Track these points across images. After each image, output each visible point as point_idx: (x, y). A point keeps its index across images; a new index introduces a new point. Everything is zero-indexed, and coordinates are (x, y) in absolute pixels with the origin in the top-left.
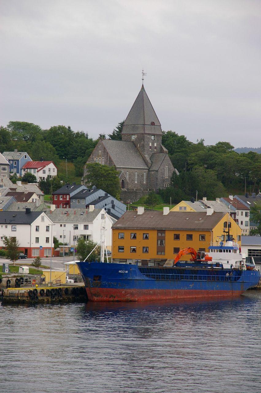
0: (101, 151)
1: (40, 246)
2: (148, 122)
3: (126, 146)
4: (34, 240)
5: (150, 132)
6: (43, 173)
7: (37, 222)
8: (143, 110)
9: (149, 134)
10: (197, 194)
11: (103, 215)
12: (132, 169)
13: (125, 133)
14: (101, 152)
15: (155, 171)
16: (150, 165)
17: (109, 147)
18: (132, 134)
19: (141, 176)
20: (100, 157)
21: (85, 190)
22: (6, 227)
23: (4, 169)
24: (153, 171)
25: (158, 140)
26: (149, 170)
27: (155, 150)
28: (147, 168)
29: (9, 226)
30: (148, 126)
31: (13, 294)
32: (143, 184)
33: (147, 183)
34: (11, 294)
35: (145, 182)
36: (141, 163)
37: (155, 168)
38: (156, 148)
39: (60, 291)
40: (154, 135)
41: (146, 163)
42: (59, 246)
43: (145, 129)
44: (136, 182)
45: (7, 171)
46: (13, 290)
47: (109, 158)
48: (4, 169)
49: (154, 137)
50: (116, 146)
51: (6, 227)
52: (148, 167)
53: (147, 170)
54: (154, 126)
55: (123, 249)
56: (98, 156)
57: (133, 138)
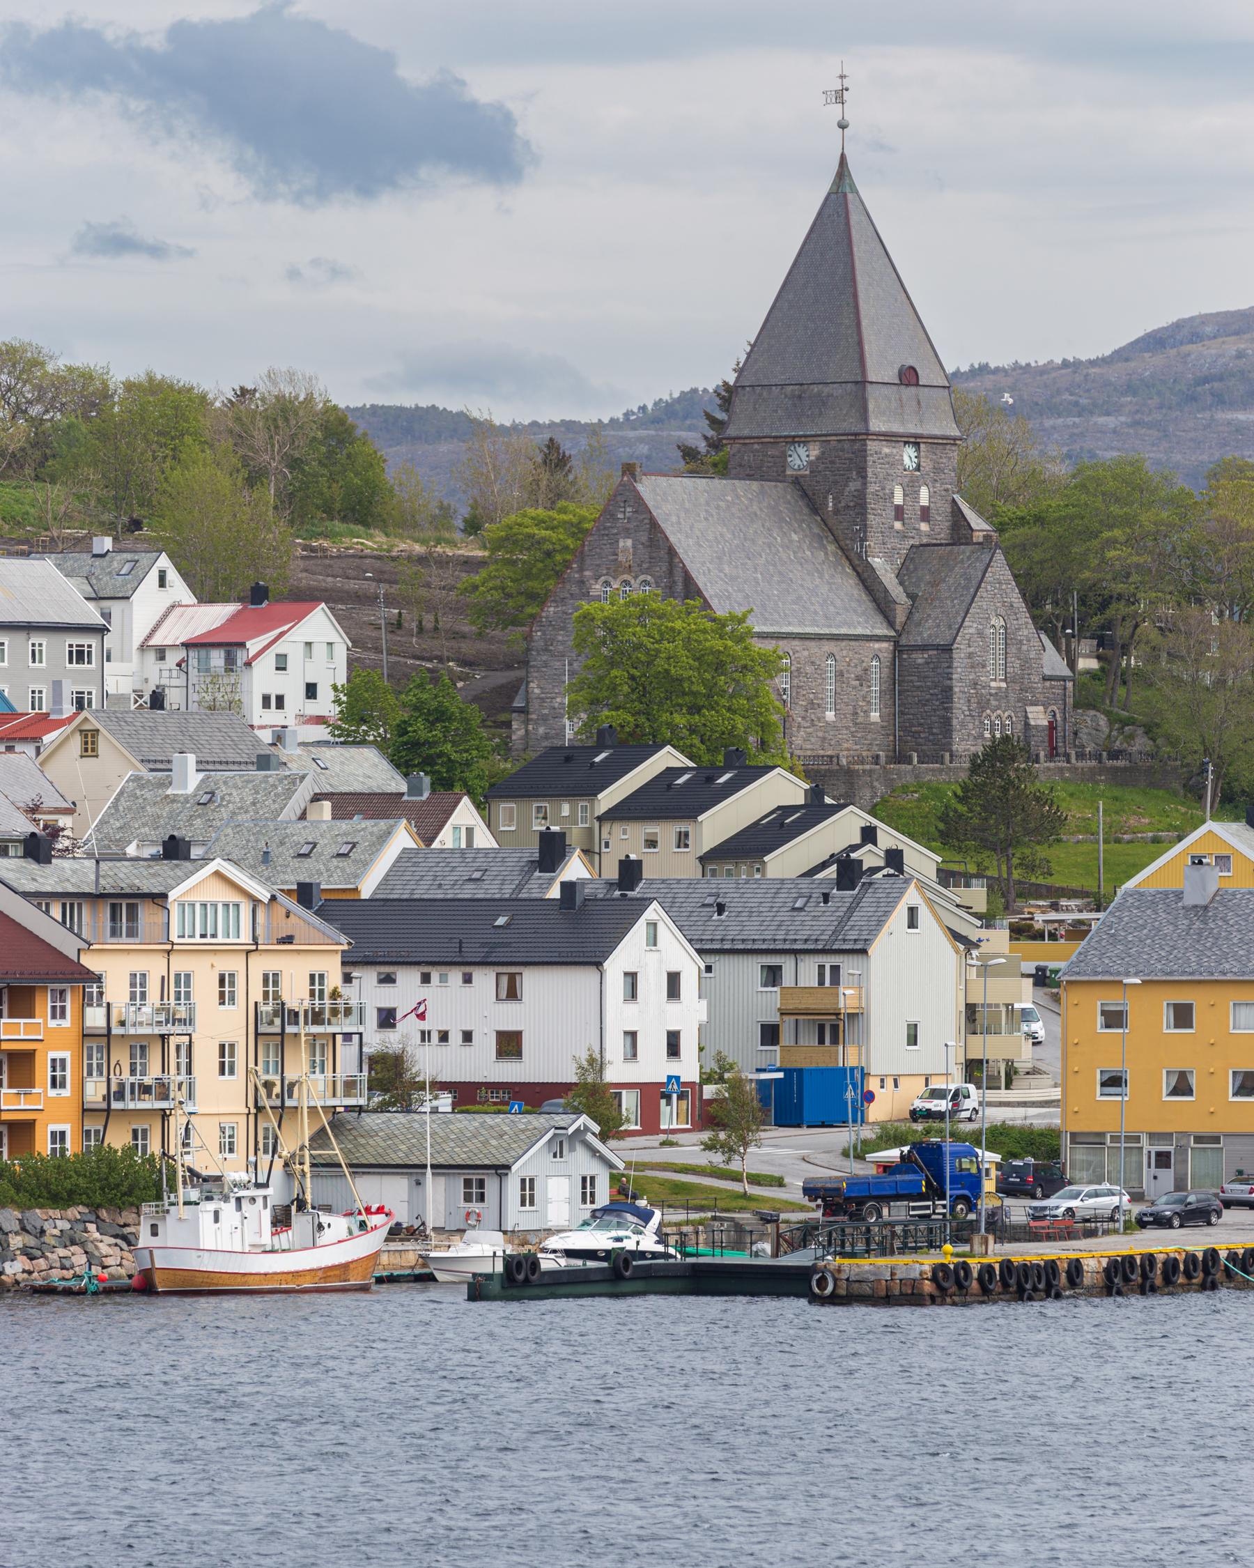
0: (629, 543)
1: (670, 1078)
2: (881, 368)
3: (761, 510)
4: (615, 1047)
5: (896, 428)
6: (277, 669)
7: (629, 952)
8: (851, 300)
9: (890, 437)
10: (1211, 777)
11: (912, 911)
12: (807, 643)
13: (746, 432)
14: (634, 546)
15: (937, 647)
16: (900, 618)
17: (674, 519)
18: (794, 440)
19: (858, 678)
20: (626, 577)
21: (685, 770)
22: (468, 979)
23: (80, 655)
24: (924, 648)
25: (938, 470)
26: (896, 644)
27: (924, 527)
28: (879, 632)
29: (485, 980)
30: (886, 391)
31: (864, 1286)
32: (867, 727)
33: (889, 718)
34: (857, 1285)
35: (875, 716)
36: (854, 605)
37: (927, 632)
38: (925, 514)
39: (962, 1273)
40: (915, 441)
41: (882, 604)
42: (780, 1075)
43: (871, 406)
44: (830, 715)
45: (93, 665)
46: (867, 1268)
47: (679, 579)
48: (80, 655)
49: (918, 450)
50: (714, 512)
51: (468, 979)
52: (891, 624)
53: (885, 645)
54: (913, 389)
55: (1183, 1076)
56: (616, 569)
57: (801, 458)
